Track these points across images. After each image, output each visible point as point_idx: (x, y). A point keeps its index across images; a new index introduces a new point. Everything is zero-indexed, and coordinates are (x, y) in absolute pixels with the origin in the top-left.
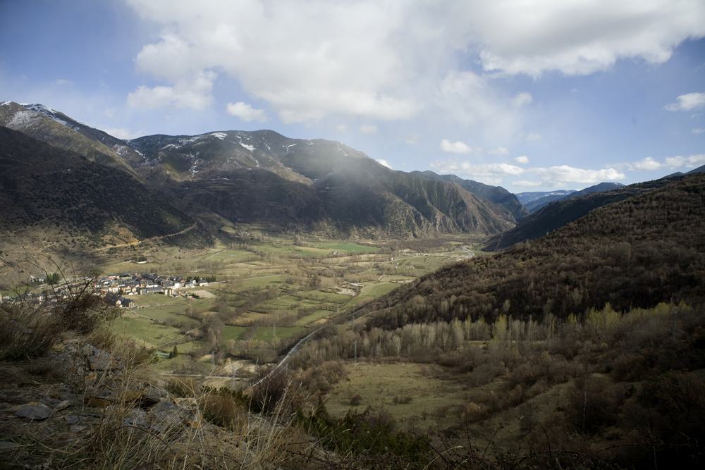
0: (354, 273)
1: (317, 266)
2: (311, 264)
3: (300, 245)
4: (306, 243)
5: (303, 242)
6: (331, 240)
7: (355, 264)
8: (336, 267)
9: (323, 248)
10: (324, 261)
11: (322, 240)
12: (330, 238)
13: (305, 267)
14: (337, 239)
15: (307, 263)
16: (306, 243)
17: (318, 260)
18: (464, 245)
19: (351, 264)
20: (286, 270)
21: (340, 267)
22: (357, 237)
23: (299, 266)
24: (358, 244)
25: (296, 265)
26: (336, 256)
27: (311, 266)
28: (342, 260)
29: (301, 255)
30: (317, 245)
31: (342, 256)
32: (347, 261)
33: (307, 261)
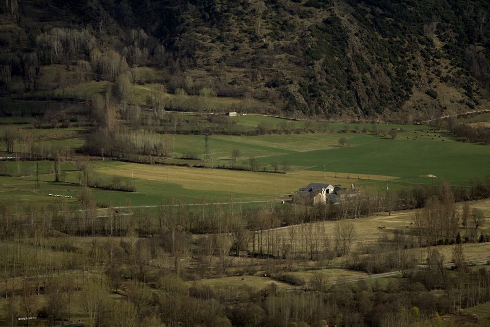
0: (443, 309)
1: (222, 270)
2: (185, 261)
3: (119, 154)
4: (153, 140)
5: (139, 139)
6: (302, 121)
7: (447, 253)
8: (333, 276)
9: (252, 167)
10: (262, 240)
11: (250, 121)
12: (290, 106)
13: (153, 282)
14: (332, 112)
15: (164, 261)
16: (153, 140)
17: (227, 241)
18: (54, 27)
19: (423, 255)
20: (41, 301)
21: (354, 277)
22: (450, 94)
23: (115, 278)
24: (460, 134)
25: (97, 273)
26: (332, 213)
27: (189, 275)
28: (366, 231)
29: (125, 211)
30: (218, 149)
31: (365, 211)
32: (398, 240)
33: (168, 247)
